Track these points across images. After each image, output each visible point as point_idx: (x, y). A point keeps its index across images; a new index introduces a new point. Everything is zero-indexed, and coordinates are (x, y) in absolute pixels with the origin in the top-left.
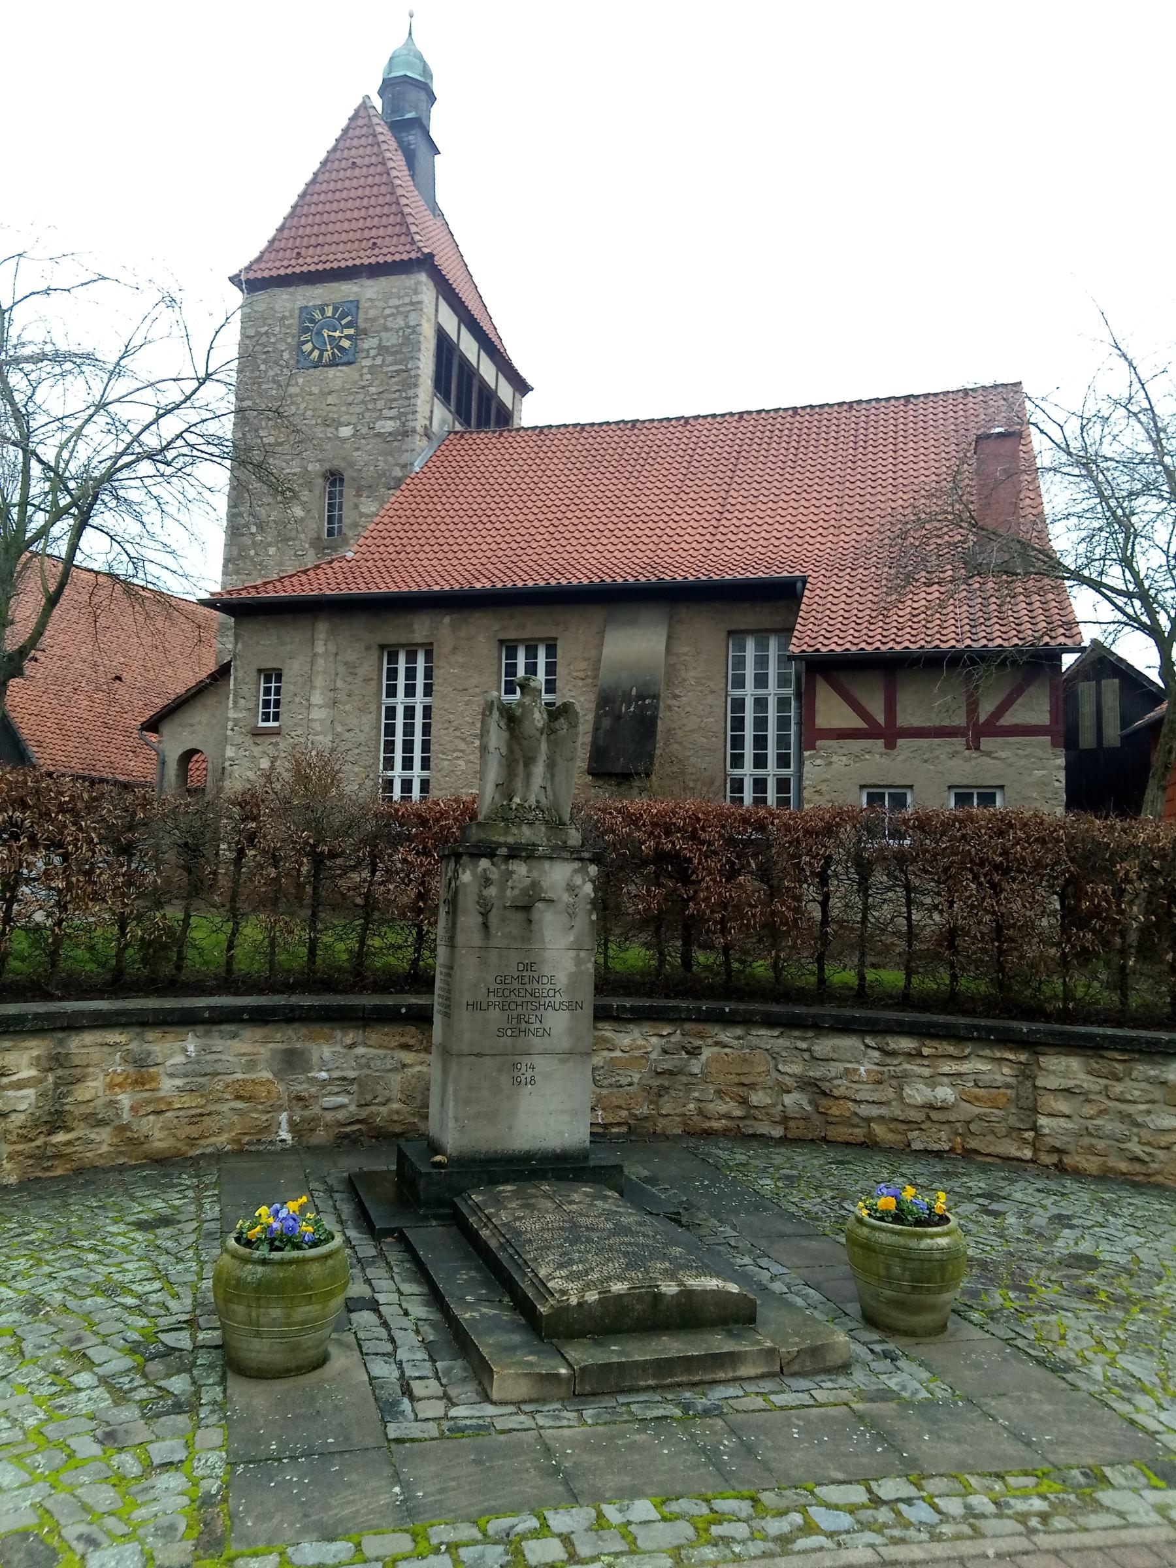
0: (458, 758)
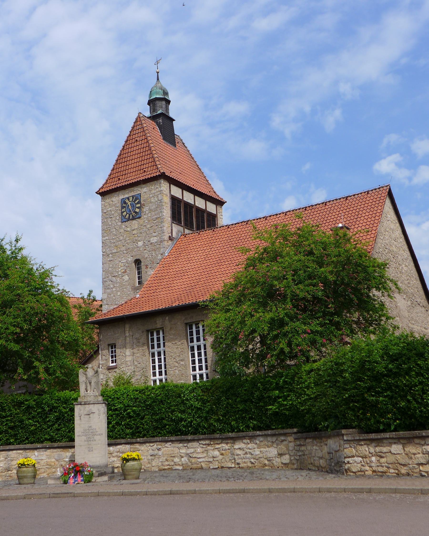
0: (175, 369)
